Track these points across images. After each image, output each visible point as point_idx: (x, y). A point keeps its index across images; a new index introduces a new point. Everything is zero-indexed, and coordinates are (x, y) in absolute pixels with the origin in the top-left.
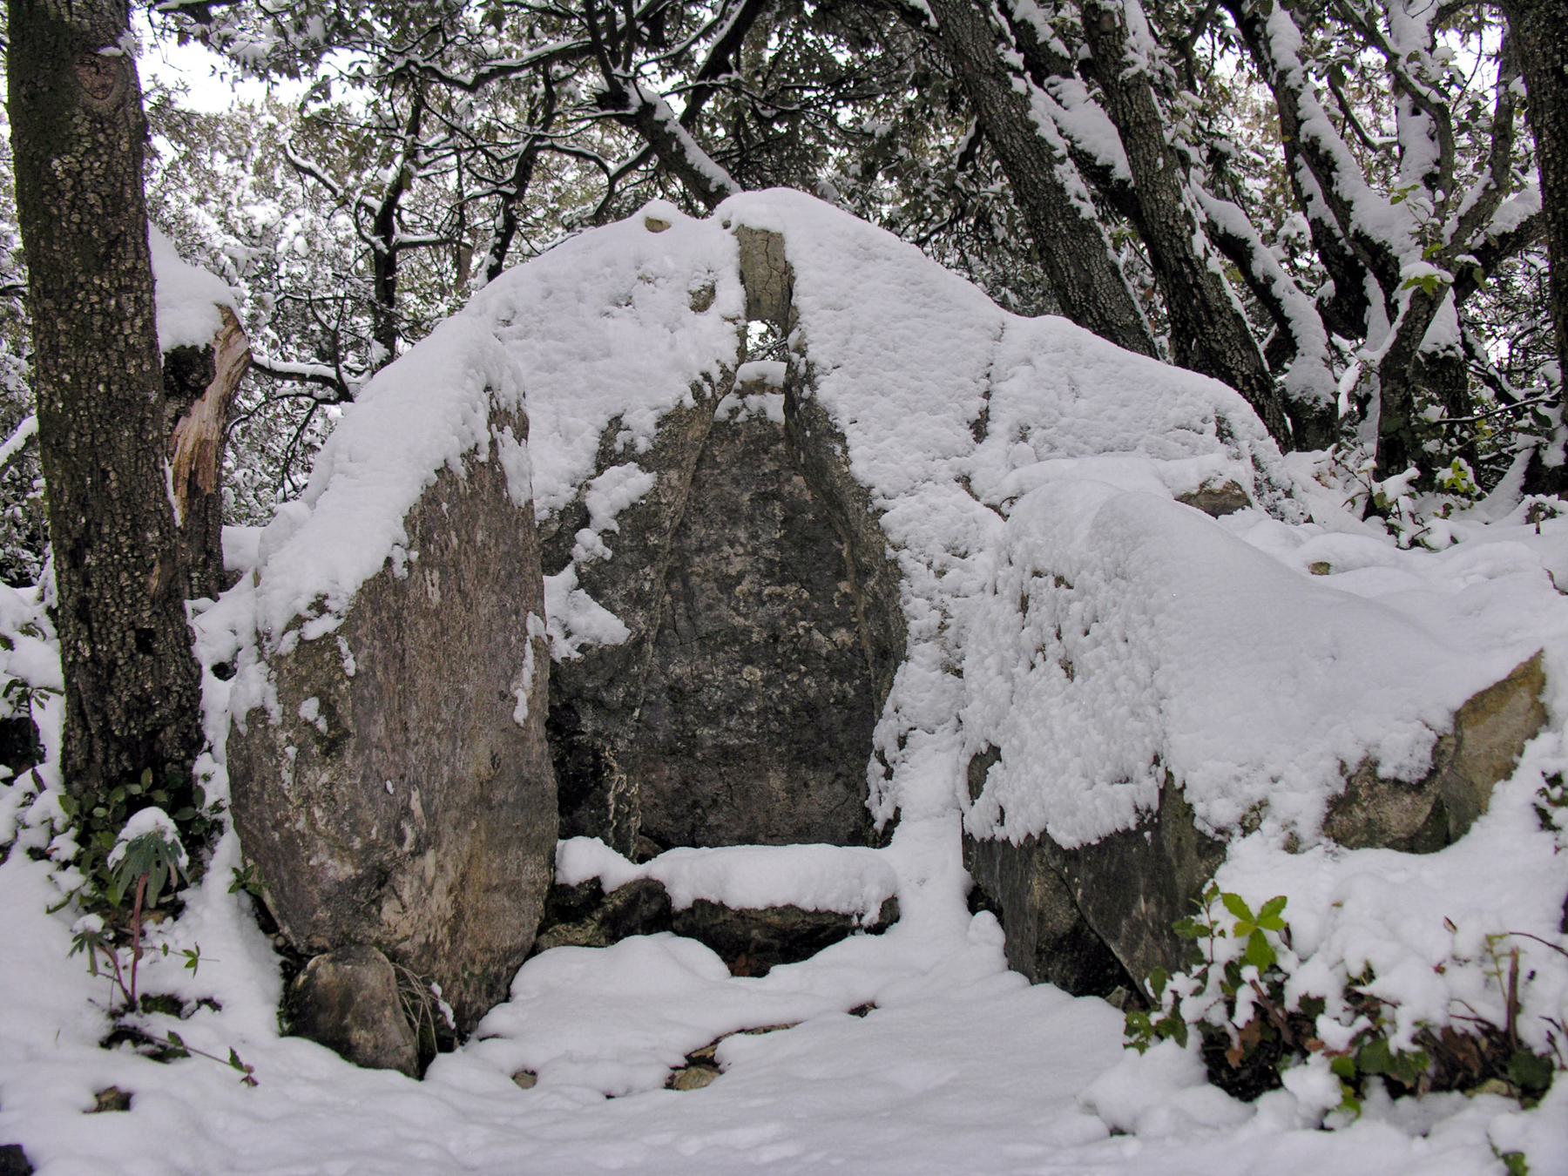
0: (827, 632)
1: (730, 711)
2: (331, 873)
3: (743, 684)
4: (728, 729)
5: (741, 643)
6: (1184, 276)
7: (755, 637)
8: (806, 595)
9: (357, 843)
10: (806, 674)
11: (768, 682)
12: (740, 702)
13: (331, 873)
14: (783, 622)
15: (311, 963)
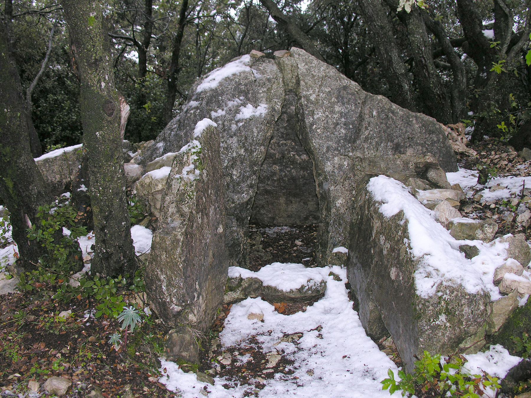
0: (300, 156)
1: (268, 179)
2: (176, 310)
3: (273, 171)
4: (268, 184)
5: (272, 158)
6: (422, 62)
7: (277, 156)
8: (293, 144)
9: (184, 304)
10: (293, 168)
11: (281, 170)
12: (271, 176)
13: (176, 310)
14: (286, 152)
15: (170, 332)
